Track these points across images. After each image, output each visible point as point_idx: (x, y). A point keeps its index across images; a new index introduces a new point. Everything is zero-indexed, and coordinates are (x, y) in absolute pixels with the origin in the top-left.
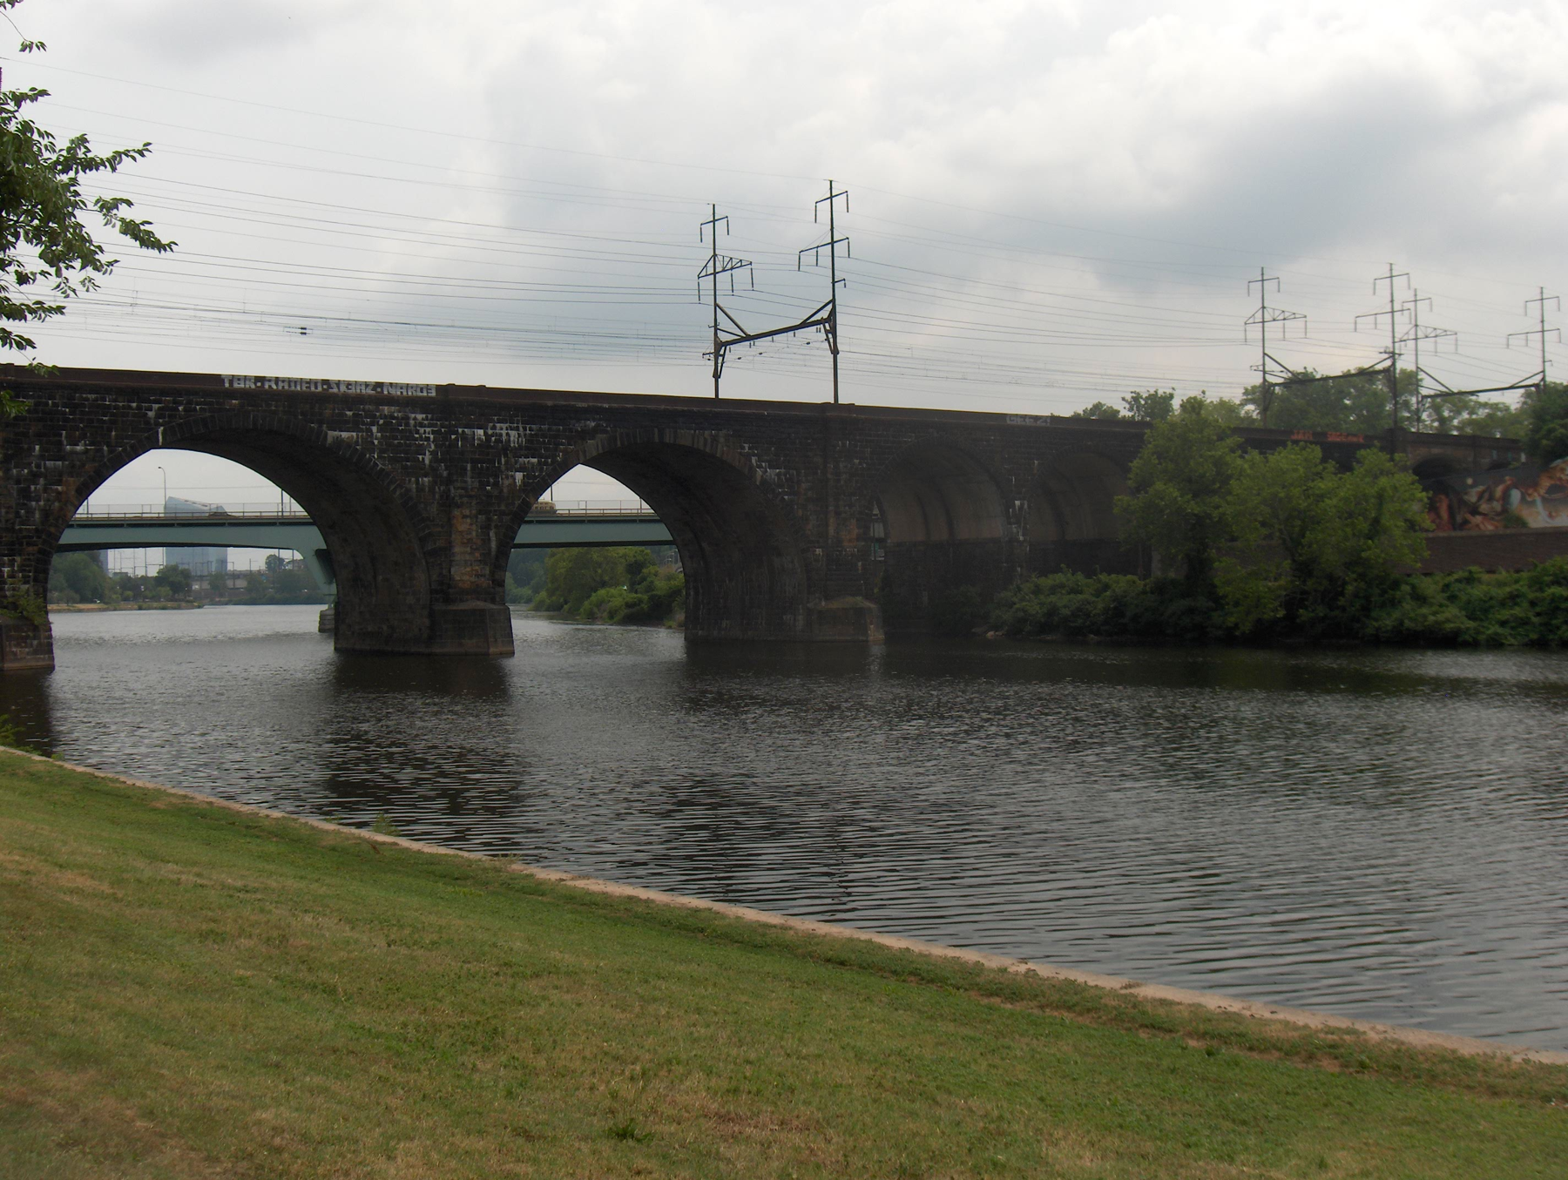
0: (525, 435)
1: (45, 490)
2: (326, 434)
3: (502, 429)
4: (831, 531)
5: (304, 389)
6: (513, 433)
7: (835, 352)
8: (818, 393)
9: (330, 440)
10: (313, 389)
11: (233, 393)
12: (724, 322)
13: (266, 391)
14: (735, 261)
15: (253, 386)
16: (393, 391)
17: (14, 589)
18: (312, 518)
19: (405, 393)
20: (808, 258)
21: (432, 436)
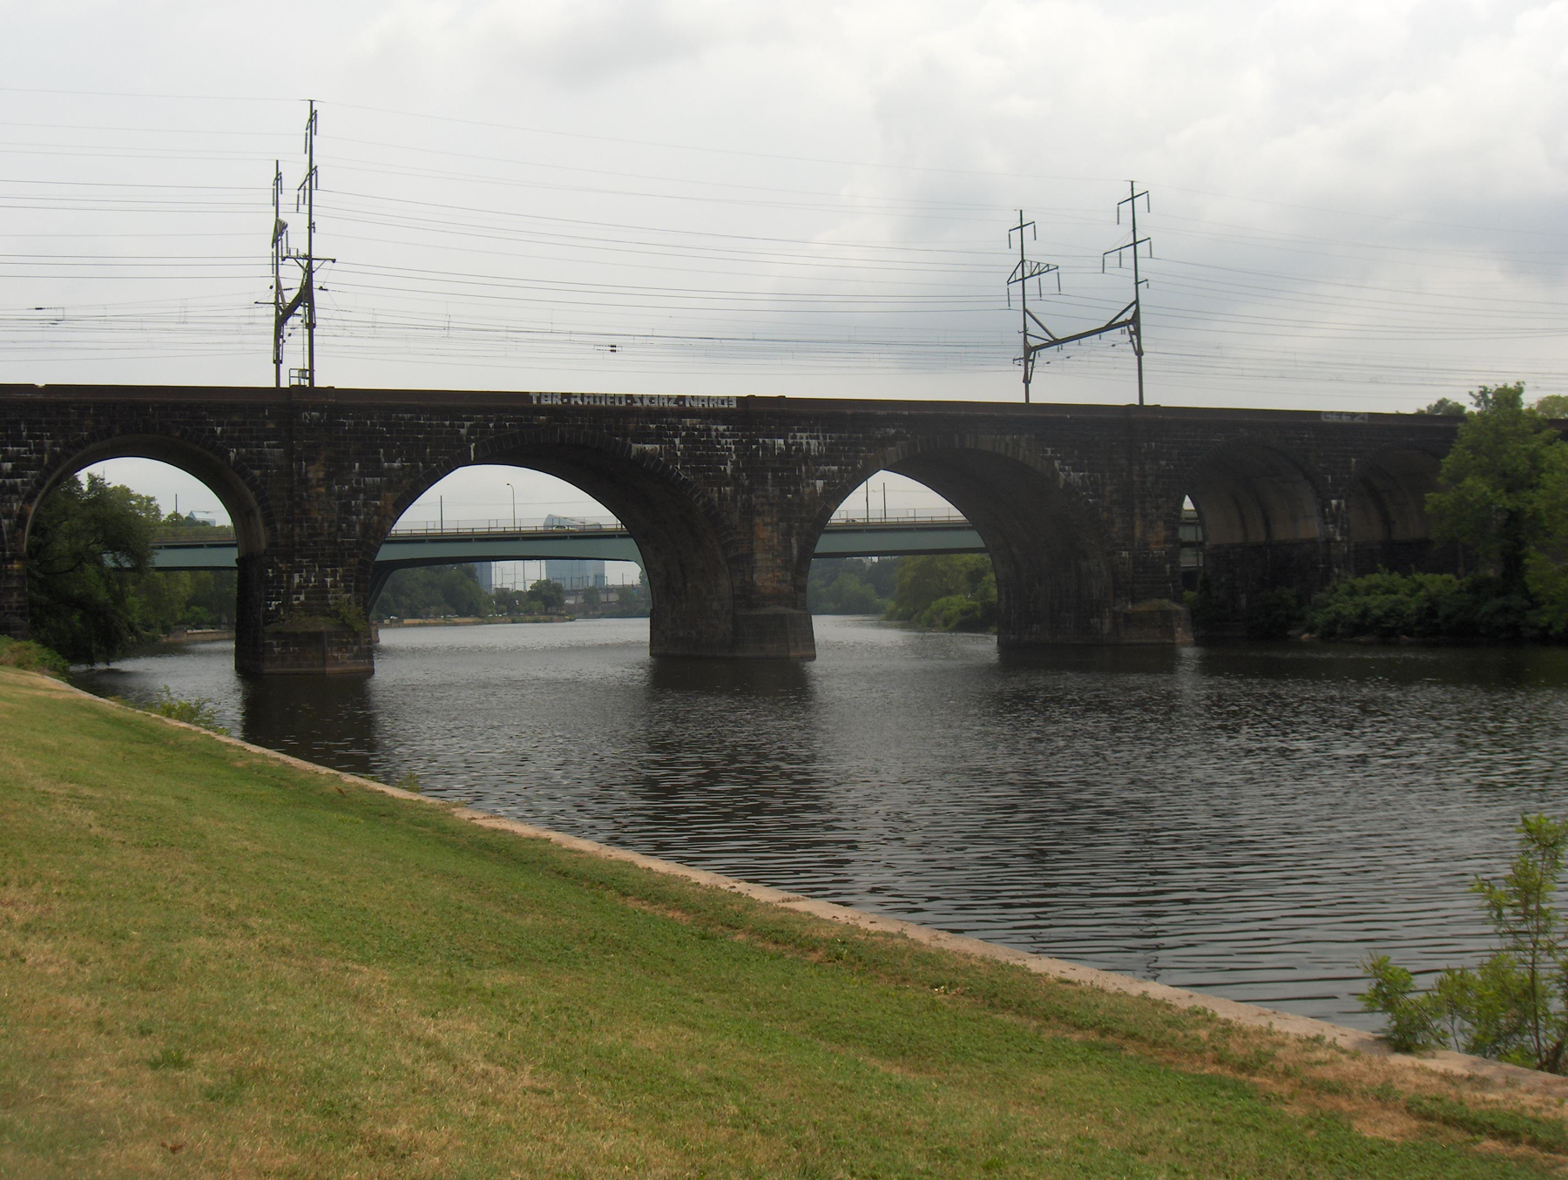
0: (825, 444)
1: (365, 505)
2: (630, 447)
3: (802, 438)
4: (1138, 533)
5: (609, 403)
6: (813, 442)
7: (1139, 353)
8: (1120, 393)
9: (634, 452)
10: (617, 404)
11: (541, 410)
12: (1033, 328)
13: (572, 406)
14: (1042, 266)
15: (560, 403)
16: (694, 404)
17: (336, 598)
18: (628, 530)
19: (706, 406)
20: (1112, 260)
21: (733, 447)
